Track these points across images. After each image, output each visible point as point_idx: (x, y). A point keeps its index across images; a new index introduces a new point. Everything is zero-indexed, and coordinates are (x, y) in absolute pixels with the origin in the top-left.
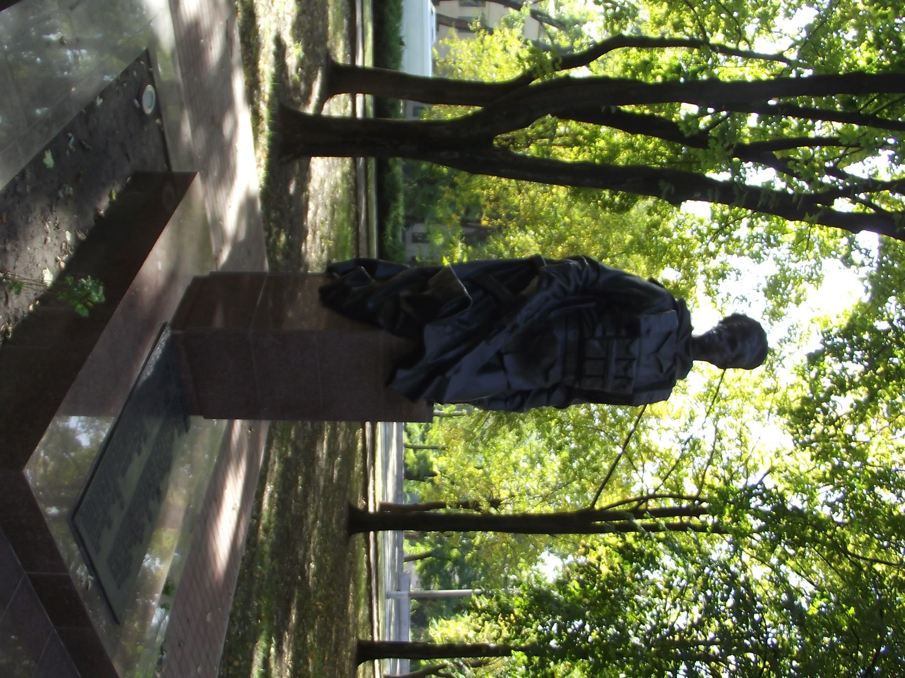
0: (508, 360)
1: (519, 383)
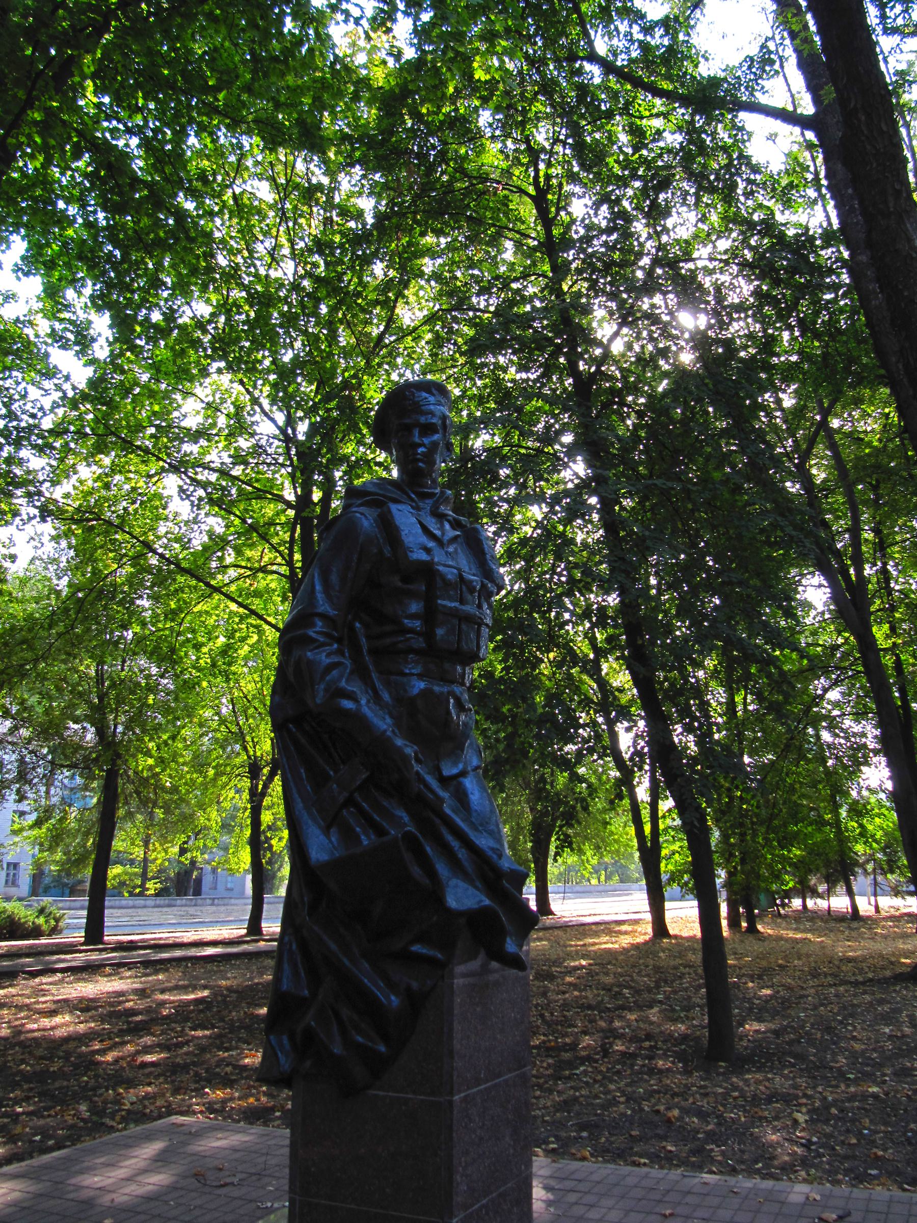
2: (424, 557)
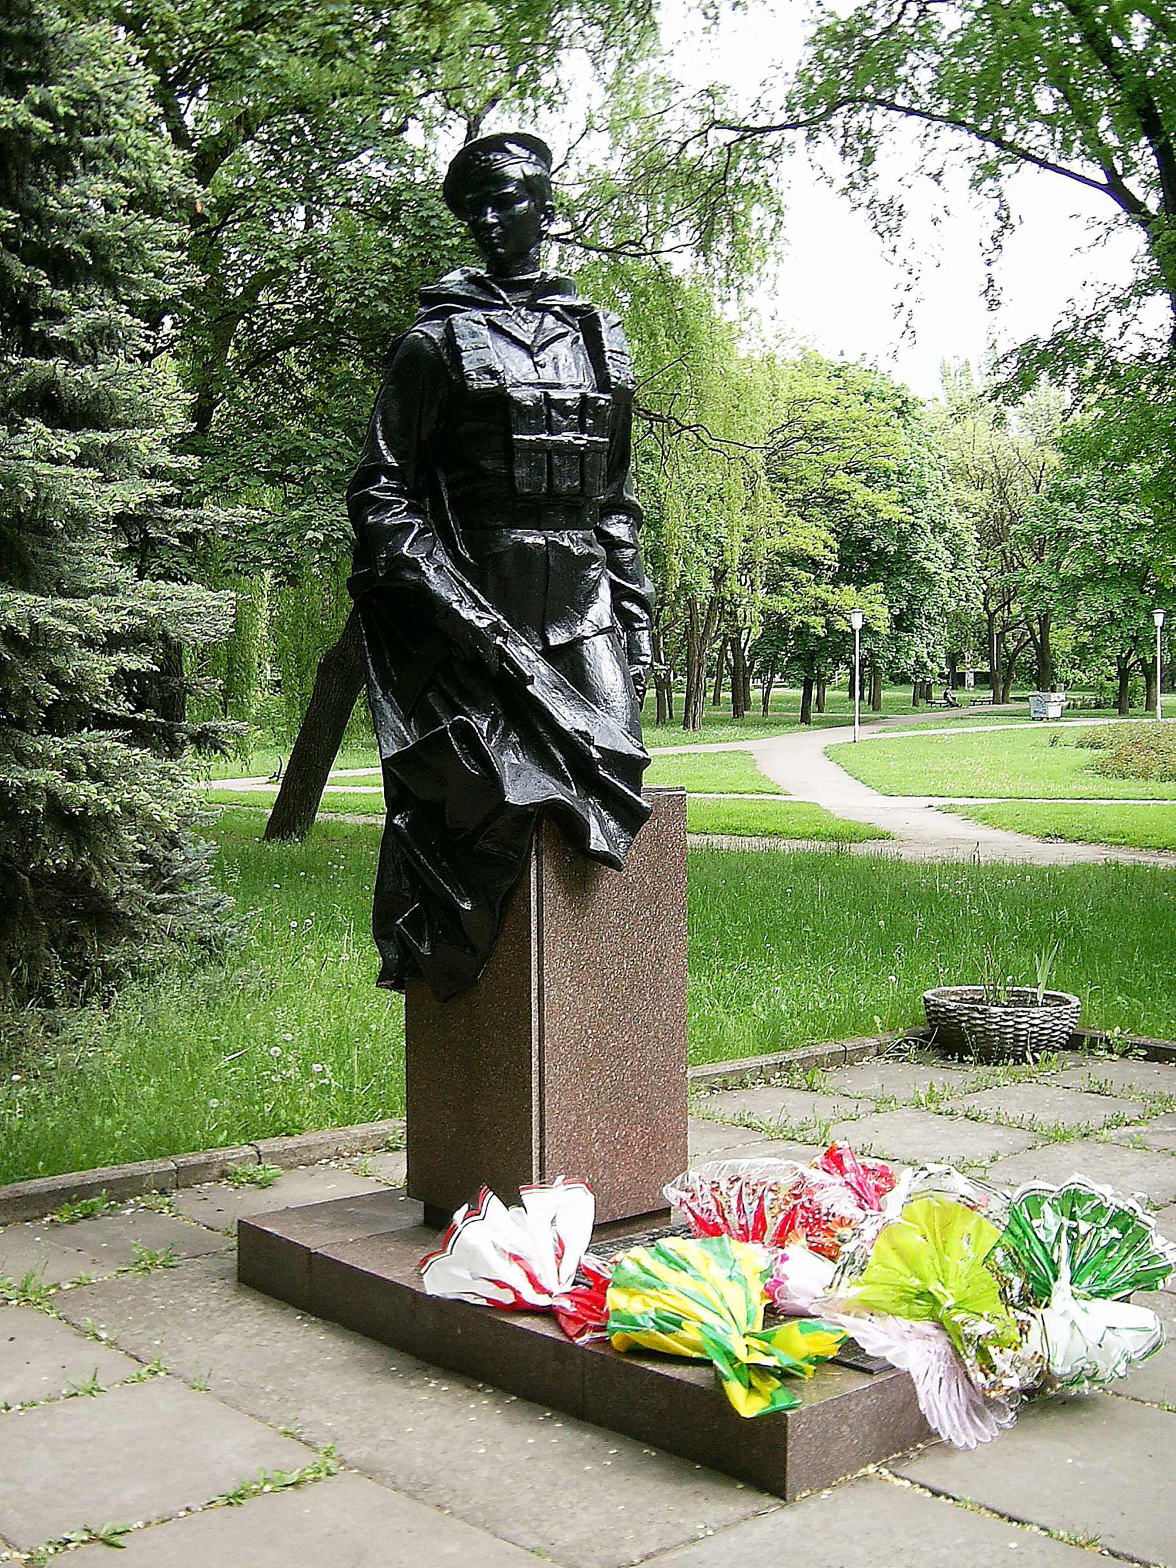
0: (557, 637)
1: (601, 610)
2: (487, 383)
